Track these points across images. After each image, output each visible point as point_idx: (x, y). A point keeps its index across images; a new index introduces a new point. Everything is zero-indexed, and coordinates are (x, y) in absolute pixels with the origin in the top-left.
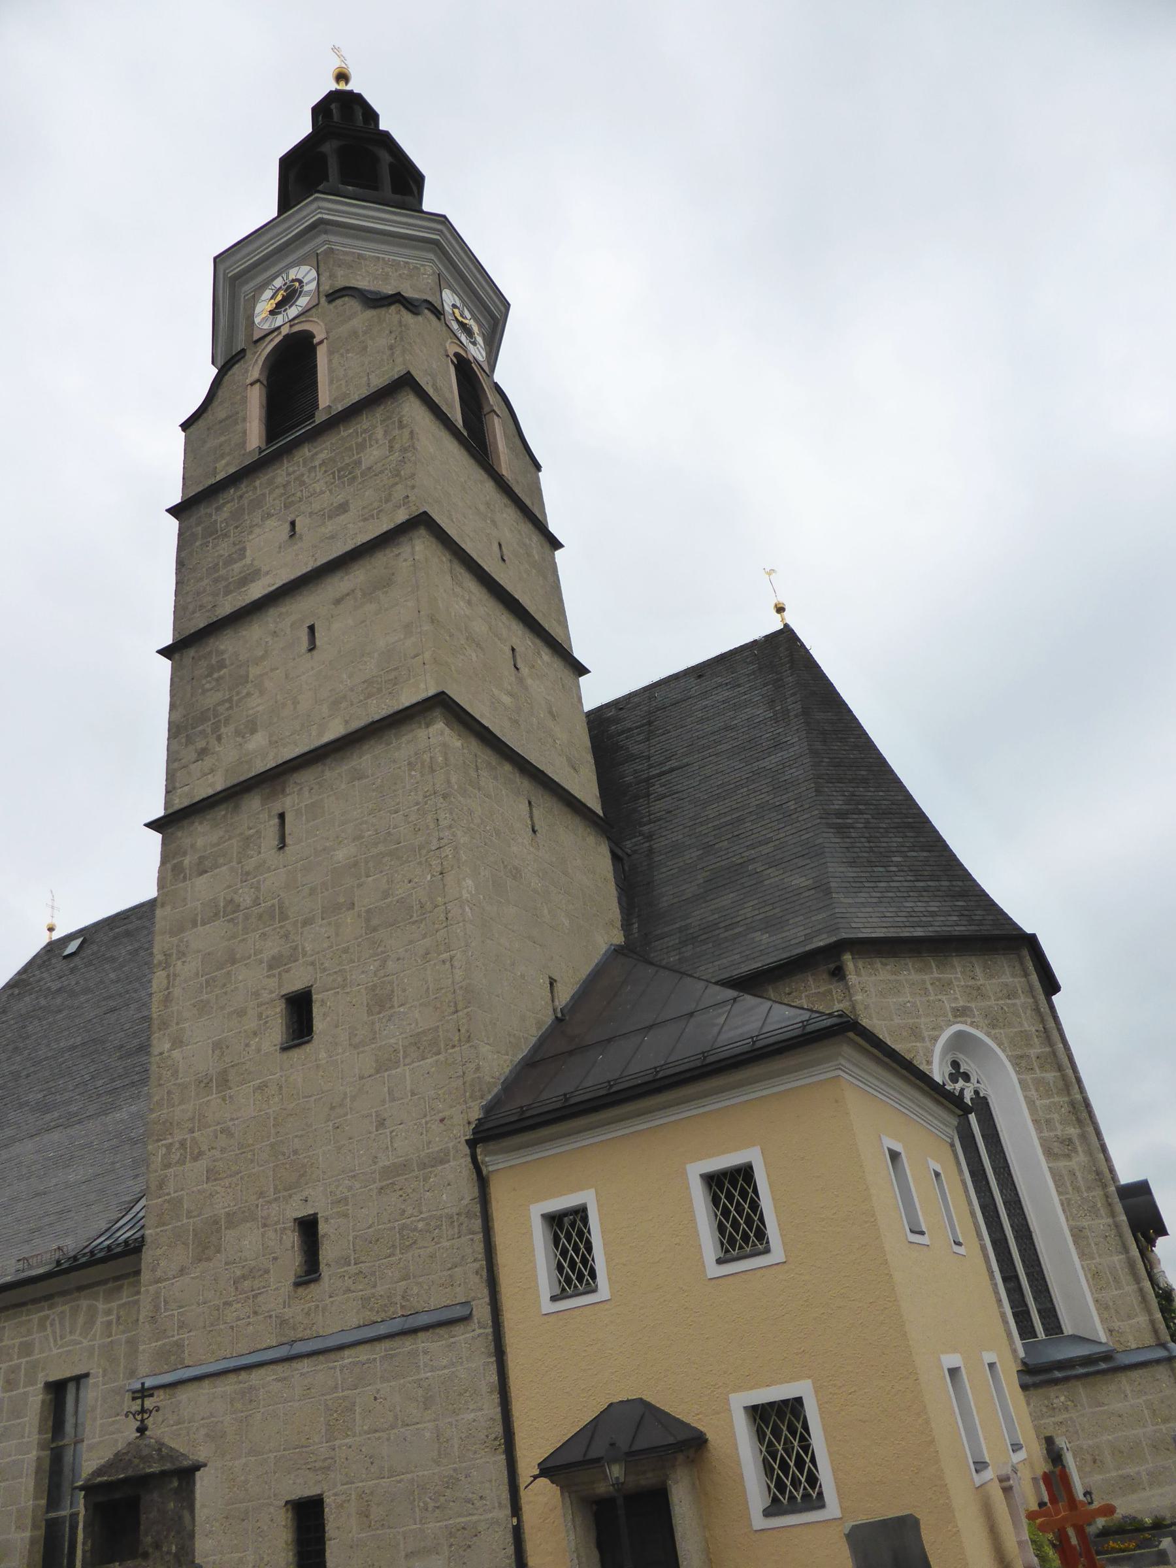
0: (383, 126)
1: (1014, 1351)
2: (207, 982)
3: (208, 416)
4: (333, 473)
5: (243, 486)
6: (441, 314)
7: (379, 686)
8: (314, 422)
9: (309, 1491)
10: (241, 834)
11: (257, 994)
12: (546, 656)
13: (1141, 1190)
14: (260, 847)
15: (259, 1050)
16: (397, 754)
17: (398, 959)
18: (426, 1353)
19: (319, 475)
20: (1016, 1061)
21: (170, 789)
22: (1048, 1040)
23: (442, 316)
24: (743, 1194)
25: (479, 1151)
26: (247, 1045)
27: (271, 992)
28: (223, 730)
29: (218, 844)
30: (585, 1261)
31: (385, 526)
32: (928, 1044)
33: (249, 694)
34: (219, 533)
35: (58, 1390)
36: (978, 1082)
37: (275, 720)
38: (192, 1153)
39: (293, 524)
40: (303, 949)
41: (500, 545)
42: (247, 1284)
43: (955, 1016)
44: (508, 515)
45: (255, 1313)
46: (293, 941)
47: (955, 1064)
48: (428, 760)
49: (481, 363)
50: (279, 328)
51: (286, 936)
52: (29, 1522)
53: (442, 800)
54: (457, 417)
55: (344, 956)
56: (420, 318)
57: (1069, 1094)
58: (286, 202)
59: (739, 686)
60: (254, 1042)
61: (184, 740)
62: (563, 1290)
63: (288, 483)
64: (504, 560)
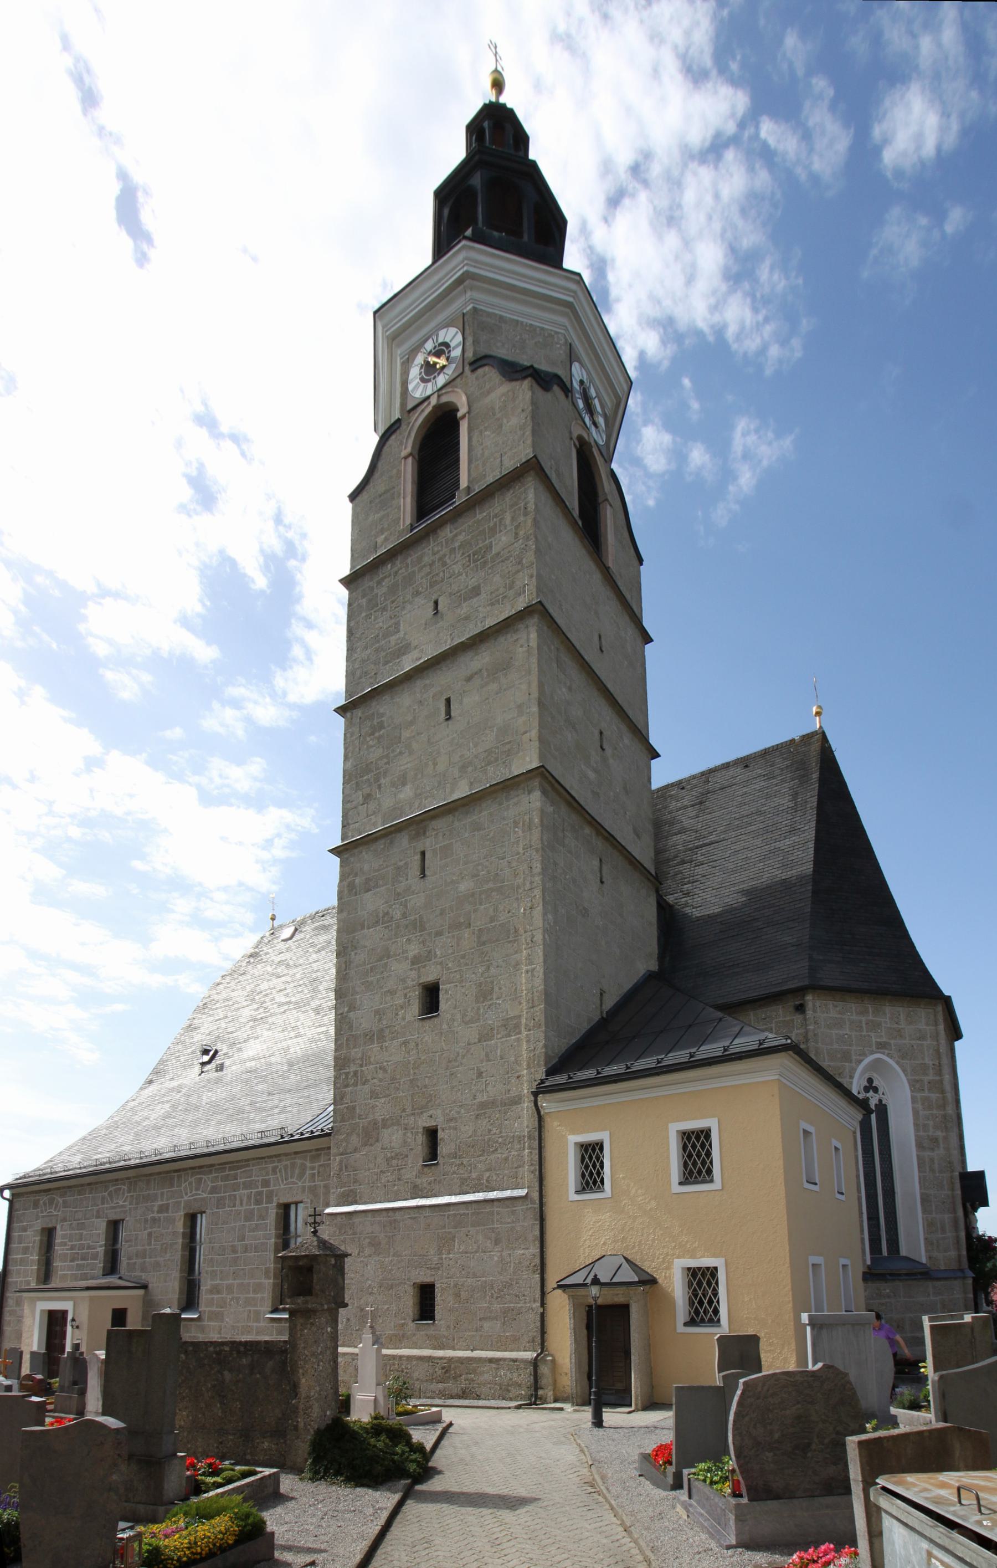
0: (532, 156)
1: (864, 1261)
2: (371, 968)
3: (370, 487)
4: (469, 556)
5: (398, 562)
6: (569, 391)
7: (496, 756)
8: (454, 502)
9: (428, 1280)
10: (395, 864)
11: (404, 981)
12: (628, 739)
13: (979, 1177)
14: (407, 875)
15: (404, 1019)
16: (506, 813)
17: (498, 967)
18: (498, 1214)
19: (459, 556)
20: (913, 1084)
21: (345, 824)
22: (939, 1071)
23: (570, 394)
24: (703, 1146)
25: (539, 1099)
26: (397, 1014)
27: (414, 981)
28: (383, 781)
29: (378, 870)
30: (599, 1174)
31: (507, 612)
32: (854, 1065)
33: (401, 753)
34: (379, 606)
35: (286, 1208)
36: (883, 1094)
37: (419, 776)
38: (361, 1079)
39: (436, 603)
40: (435, 953)
41: (600, 637)
42: (395, 1162)
43: (878, 1048)
44: (610, 607)
45: (399, 1179)
46: (428, 947)
47: (870, 1081)
48: (528, 820)
49: (601, 447)
50: (428, 397)
51: (423, 942)
52: (272, 1275)
53: (535, 853)
54: (574, 504)
55: (462, 961)
56: (549, 396)
57: (944, 1109)
58: (442, 246)
59: (773, 778)
60: (401, 1013)
61: (354, 786)
62: (687, 1178)
63: (433, 562)
64: (602, 651)
